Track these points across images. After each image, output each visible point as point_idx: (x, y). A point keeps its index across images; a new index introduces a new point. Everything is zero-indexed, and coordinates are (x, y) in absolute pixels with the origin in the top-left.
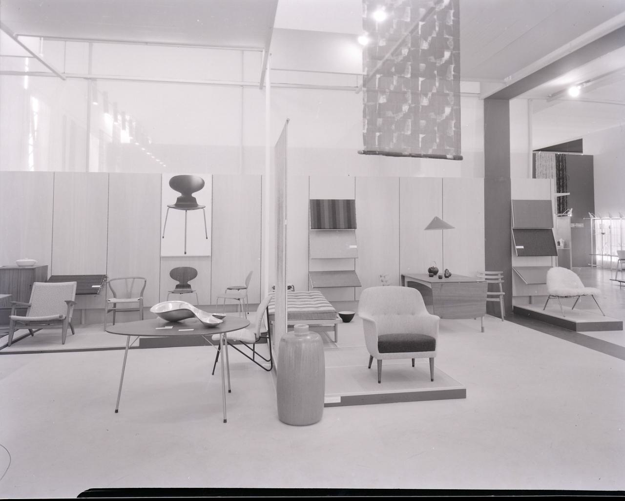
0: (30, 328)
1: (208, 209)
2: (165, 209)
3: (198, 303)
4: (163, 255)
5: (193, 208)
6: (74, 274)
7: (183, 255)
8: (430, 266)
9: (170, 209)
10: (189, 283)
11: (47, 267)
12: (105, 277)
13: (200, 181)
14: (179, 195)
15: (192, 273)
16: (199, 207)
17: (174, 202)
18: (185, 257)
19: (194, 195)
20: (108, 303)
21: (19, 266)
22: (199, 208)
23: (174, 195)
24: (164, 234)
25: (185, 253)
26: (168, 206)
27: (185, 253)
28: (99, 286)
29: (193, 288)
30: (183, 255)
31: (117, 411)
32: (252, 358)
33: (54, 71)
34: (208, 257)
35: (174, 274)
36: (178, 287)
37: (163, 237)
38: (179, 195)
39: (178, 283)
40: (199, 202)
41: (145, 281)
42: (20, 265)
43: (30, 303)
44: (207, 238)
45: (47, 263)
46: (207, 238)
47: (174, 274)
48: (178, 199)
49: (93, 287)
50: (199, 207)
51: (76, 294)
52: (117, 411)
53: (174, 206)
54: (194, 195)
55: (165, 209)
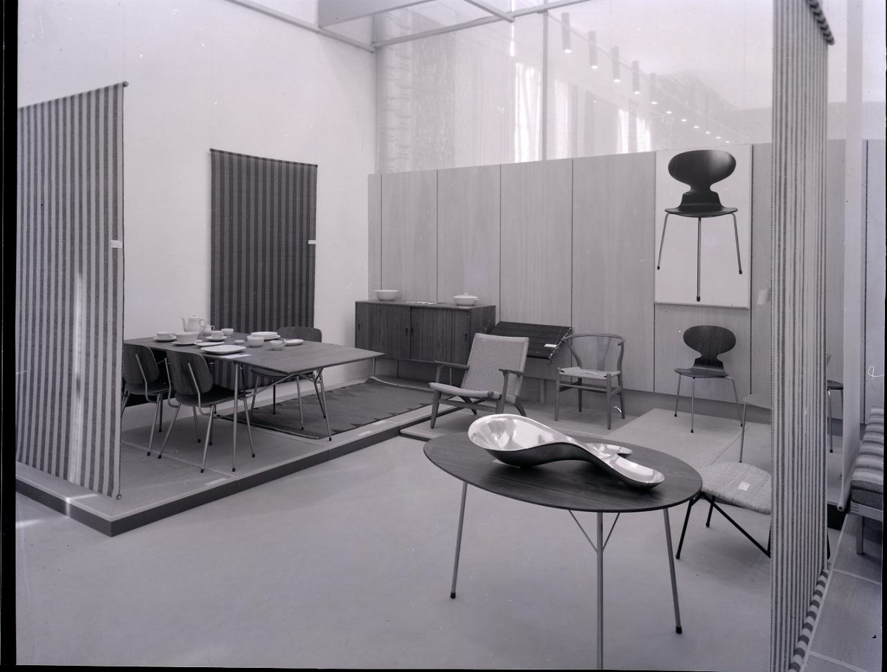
0: (474, 409)
1: (744, 217)
2: (660, 214)
3: (737, 399)
4: (659, 299)
5: (711, 213)
6: (528, 323)
7: (694, 302)
8: (681, 332)
9: (670, 215)
10: (720, 357)
11: (494, 307)
12: (567, 330)
13: (727, 160)
14: (686, 188)
15: (726, 340)
16: (724, 210)
17: (678, 202)
18: (698, 306)
19: (714, 188)
20: (560, 375)
21: (381, 300)
22: (725, 214)
23: (675, 191)
24: (659, 264)
25: (698, 299)
26: (666, 211)
27: (698, 299)
28: (554, 346)
29: (727, 368)
30: (694, 302)
31: (453, 596)
32: (766, 549)
33: (496, 14)
34: (744, 309)
35: (693, 337)
36: (698, 362)
37: (658, 268)
38: (686, 188)
39: (699, 355)
40: (724, 201)
41: (622, 344)
42: (382, 297)
43: (468, 364)
44: (741, 272)
45: (495, 302)
46: (741, 272)
47: (693, 337)
48: (684, 196)
49: (547, 345)
50: (724, 210)
51: (528, 356)
52: (453, 596)
53: (677, 211)
54: (714, 188)
55: (660, 214)
